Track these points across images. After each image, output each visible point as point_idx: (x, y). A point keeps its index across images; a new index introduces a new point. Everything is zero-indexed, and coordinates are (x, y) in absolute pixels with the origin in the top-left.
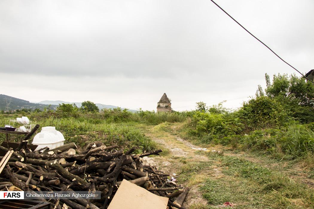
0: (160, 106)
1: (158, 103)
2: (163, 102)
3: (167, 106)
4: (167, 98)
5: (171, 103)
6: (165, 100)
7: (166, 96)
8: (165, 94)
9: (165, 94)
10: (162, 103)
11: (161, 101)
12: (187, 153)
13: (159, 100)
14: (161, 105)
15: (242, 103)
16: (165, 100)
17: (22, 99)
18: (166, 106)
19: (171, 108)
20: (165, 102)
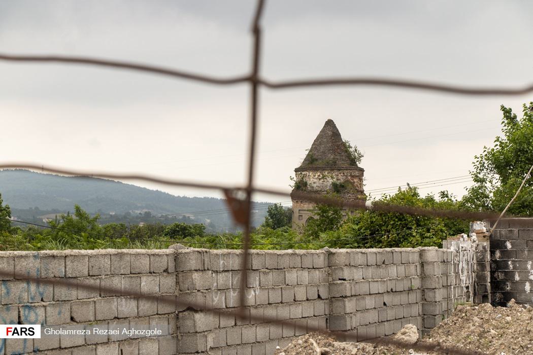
0: (305, 184)
1: (296, 170)
2: (319, 163)
3: (342, 186)
4: (344, 144)
5: (362, 170)
6: (332, 153)
7: (336, 134)
8: (330, 124)
9: (330, 124)
10: (315, 169)
11: (311, 163)
12: (369, 302)
13: (303, 155)
14: (313, 180)
15: (347, 140)
16: (332, 153)
17: (316, 137)
18: (334, 185)
19: (362, 192)
20: (332, 166)
